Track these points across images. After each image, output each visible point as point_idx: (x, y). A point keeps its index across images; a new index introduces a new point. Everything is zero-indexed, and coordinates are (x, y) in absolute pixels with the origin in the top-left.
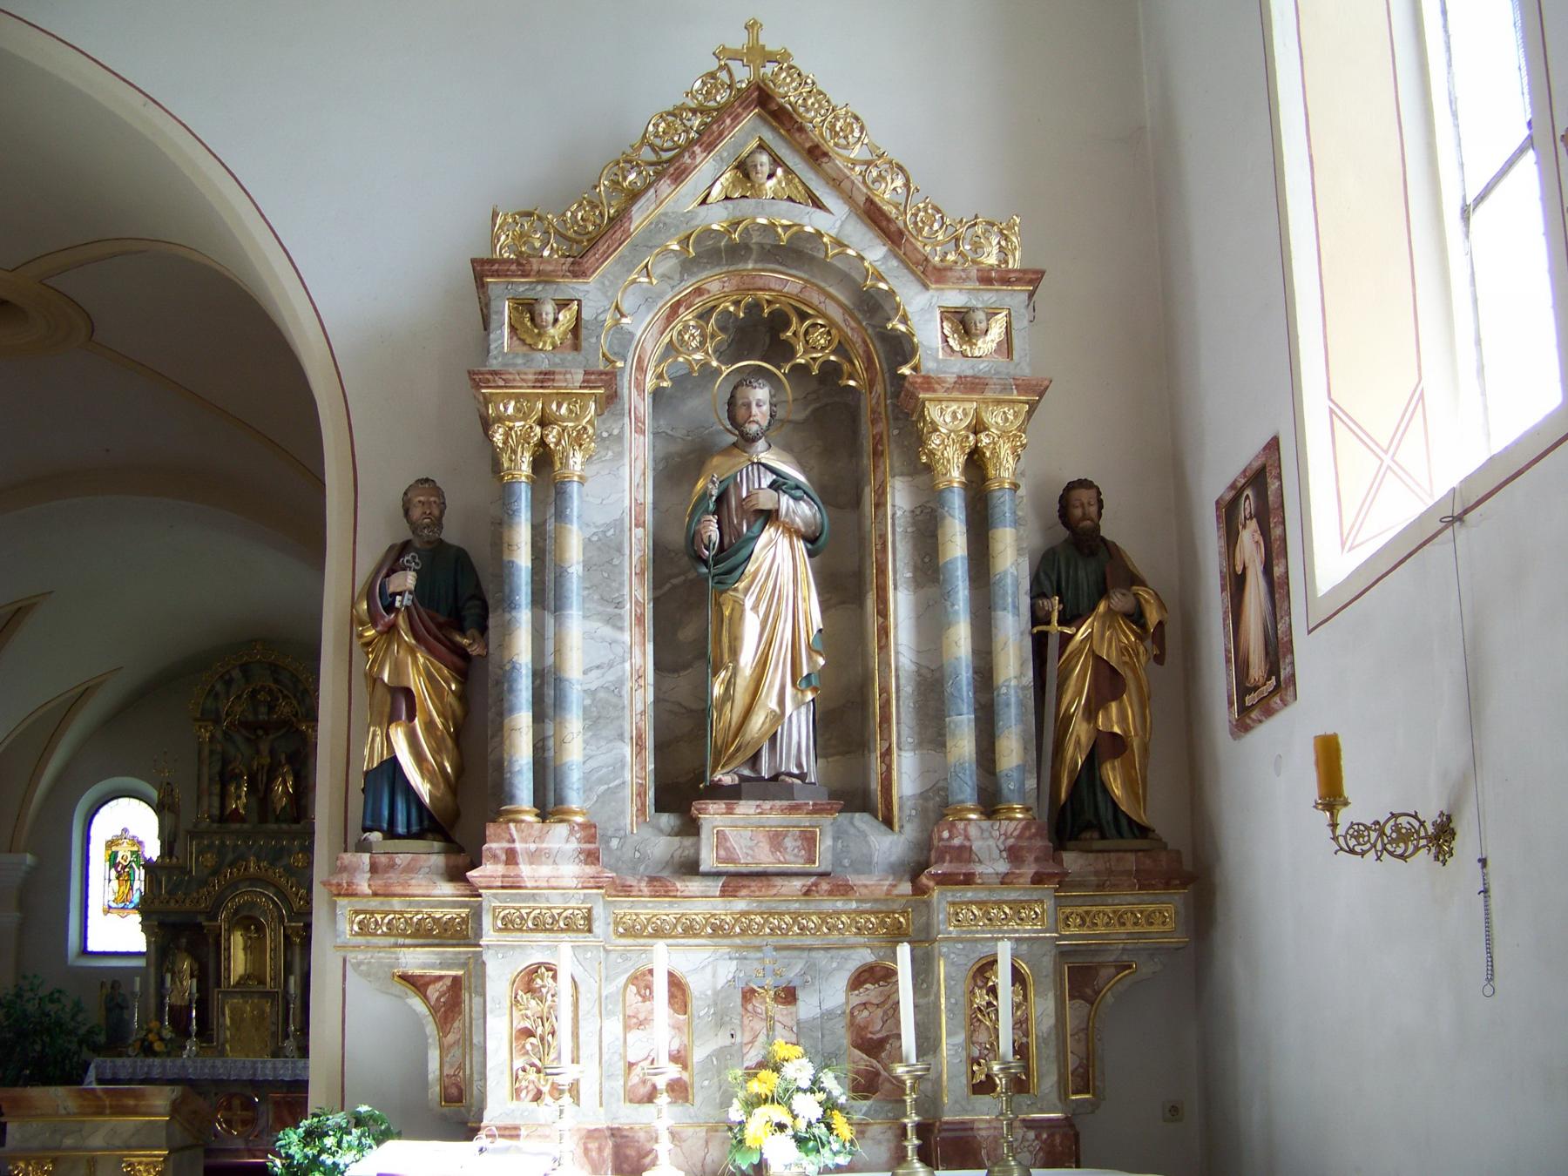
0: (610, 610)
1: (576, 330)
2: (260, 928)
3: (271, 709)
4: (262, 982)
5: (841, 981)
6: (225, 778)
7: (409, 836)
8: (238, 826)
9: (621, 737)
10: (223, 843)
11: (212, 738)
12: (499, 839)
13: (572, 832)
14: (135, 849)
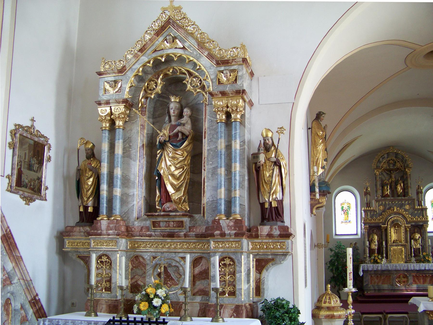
3: (394, 165)
4: (401, 242)
6: (383, 186)
10: (385, 203)
11: (379, 174)
14: (348, 205)
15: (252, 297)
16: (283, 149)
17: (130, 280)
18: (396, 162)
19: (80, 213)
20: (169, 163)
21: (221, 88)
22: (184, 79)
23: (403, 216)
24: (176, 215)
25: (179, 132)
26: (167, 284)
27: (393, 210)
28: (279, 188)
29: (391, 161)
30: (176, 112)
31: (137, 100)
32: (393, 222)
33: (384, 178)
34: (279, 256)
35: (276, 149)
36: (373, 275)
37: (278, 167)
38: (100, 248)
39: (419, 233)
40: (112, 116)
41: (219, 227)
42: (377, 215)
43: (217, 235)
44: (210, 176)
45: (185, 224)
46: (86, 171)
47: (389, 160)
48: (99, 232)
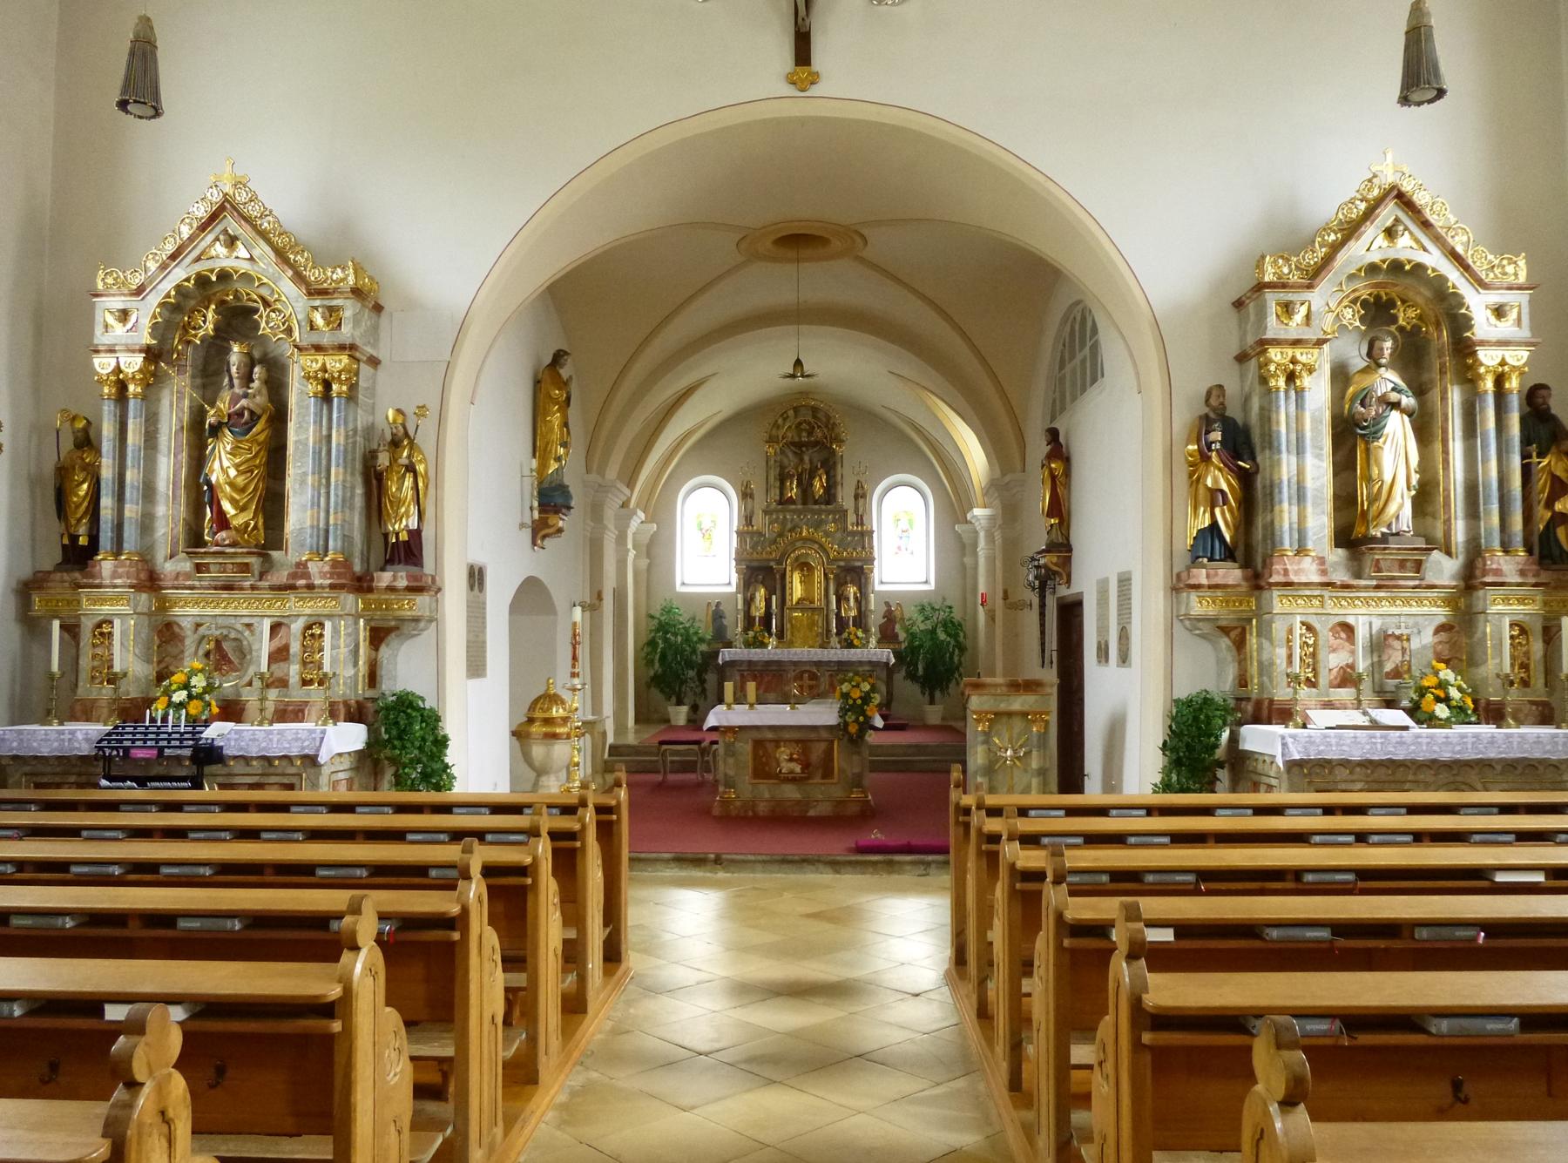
0: (1318, 451)
1: (1308, 317)
2: (810, 569)
3: (810, 434)
5: (1430, 630)
7: (1221, 560)
8: (793, 507)
9: (1323, 513)
10: (785, 517)
11: (775, 453)
12: (1279, 563)
13: (1313, 561)
15: (362, 690)
16: (425, 439)
17: (155, 664)
18: (814, 428)
19: (64, 547)
20: (226, 463)
21: (315, 338)
22: (256, 311)
23: (821, 546)
24: (235, 553)
25: (243, 408)
26: (220, 669)
27: (801, 533)
28: (413, 510)
29: (804, 426)
30: (242, 371)
31: (169, 347)
32: (797, 559)
33: (786, 461)
34: (406, 623)
35: (411, 442)
36: (745, 673)
37: (412, 474)
38: (98, 610)
39: (854, 584)
40: (121, 376)
41: (307, 575)
42: (767, 544)
43: (302, 587)
44: (297, 486)
45: (251, 569)
46: (74, 469)
47: (800, 424)
48: (97, 581)
